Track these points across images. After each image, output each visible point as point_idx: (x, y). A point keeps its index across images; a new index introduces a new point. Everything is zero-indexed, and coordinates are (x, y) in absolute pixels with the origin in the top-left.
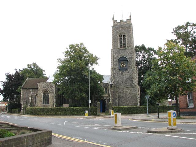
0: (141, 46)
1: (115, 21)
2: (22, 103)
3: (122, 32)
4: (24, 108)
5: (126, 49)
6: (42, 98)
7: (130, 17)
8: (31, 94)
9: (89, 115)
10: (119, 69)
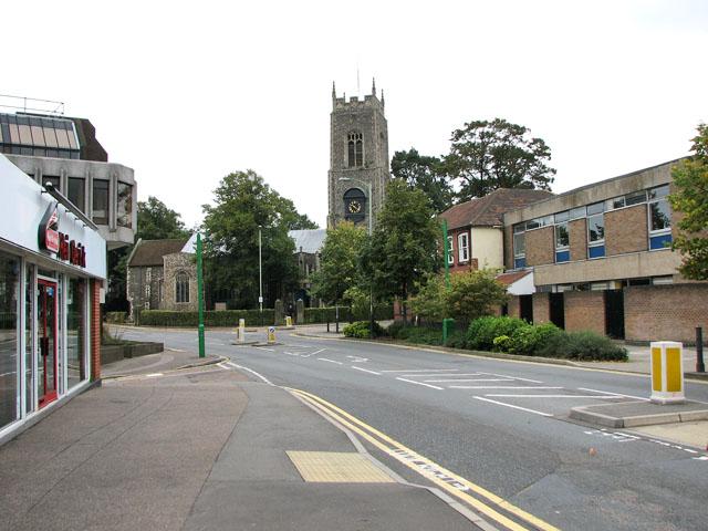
0: (408, 152)
1: (337, 101)
2: (130, 299)
3: (356, 125)
4: (135, 312)
5: (361, 169)
6: (175, 289)
7: (374, 89)
8: (149, 278)
9: (247, 325)
10: (347, 218)
